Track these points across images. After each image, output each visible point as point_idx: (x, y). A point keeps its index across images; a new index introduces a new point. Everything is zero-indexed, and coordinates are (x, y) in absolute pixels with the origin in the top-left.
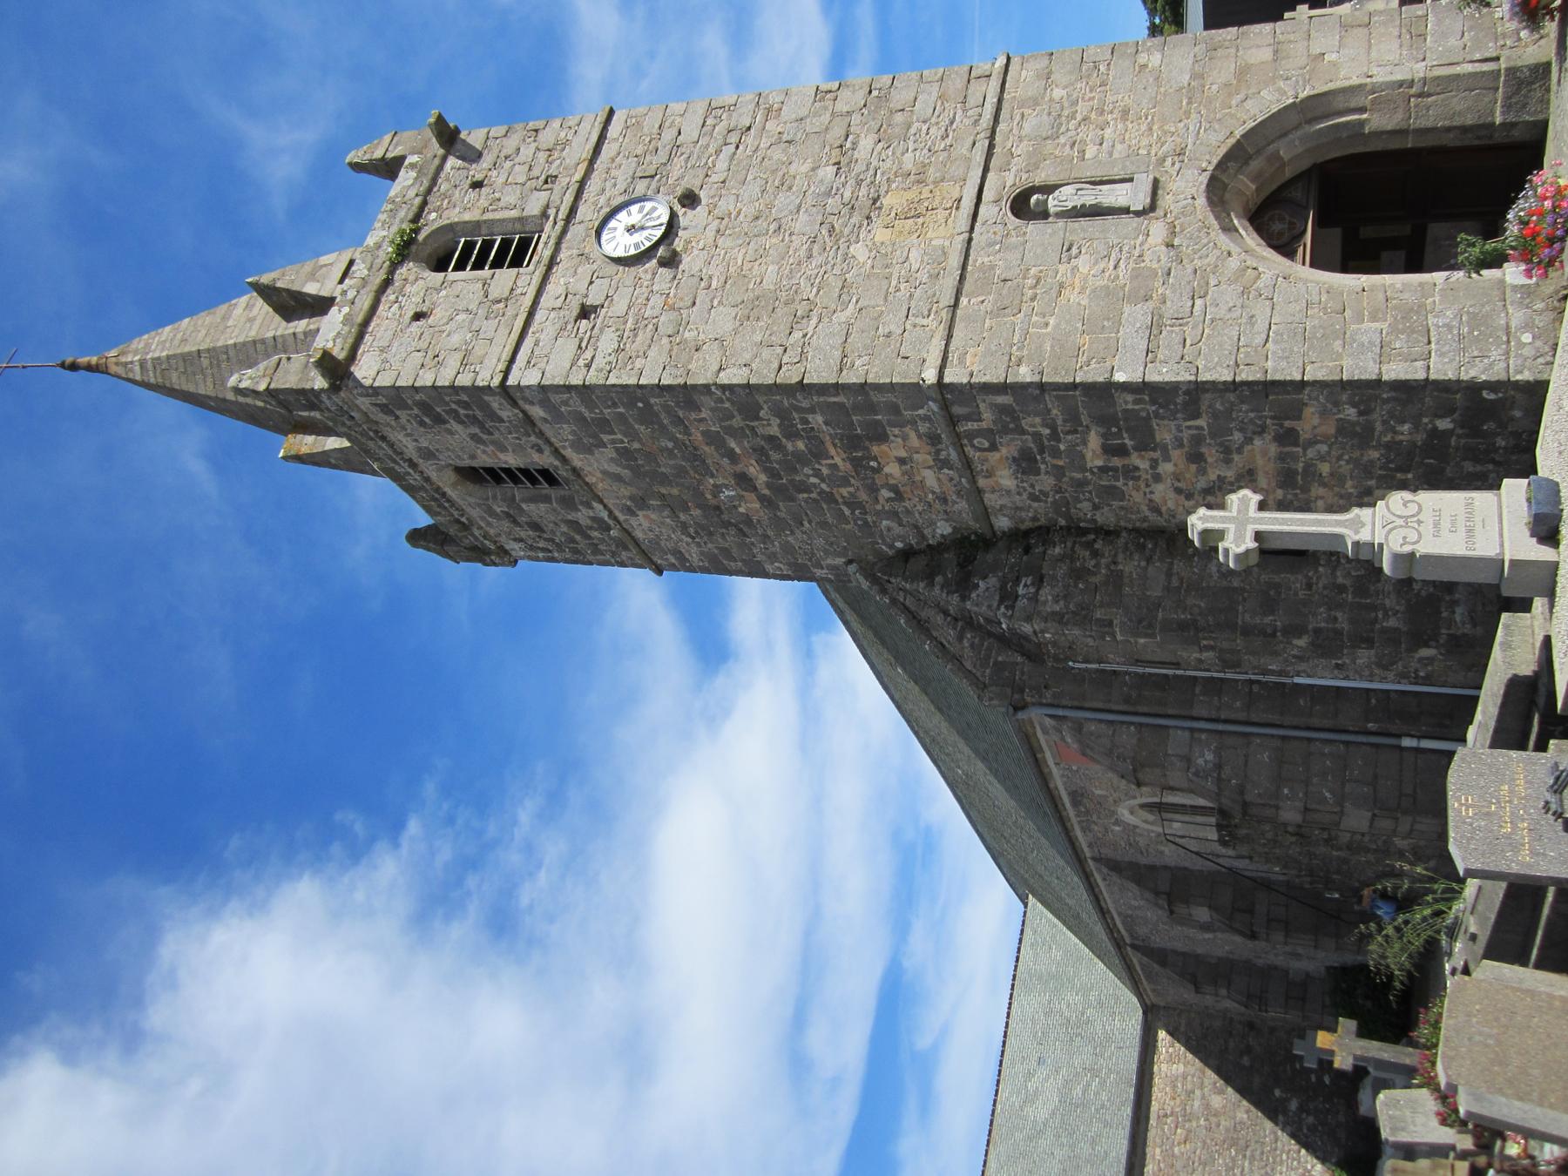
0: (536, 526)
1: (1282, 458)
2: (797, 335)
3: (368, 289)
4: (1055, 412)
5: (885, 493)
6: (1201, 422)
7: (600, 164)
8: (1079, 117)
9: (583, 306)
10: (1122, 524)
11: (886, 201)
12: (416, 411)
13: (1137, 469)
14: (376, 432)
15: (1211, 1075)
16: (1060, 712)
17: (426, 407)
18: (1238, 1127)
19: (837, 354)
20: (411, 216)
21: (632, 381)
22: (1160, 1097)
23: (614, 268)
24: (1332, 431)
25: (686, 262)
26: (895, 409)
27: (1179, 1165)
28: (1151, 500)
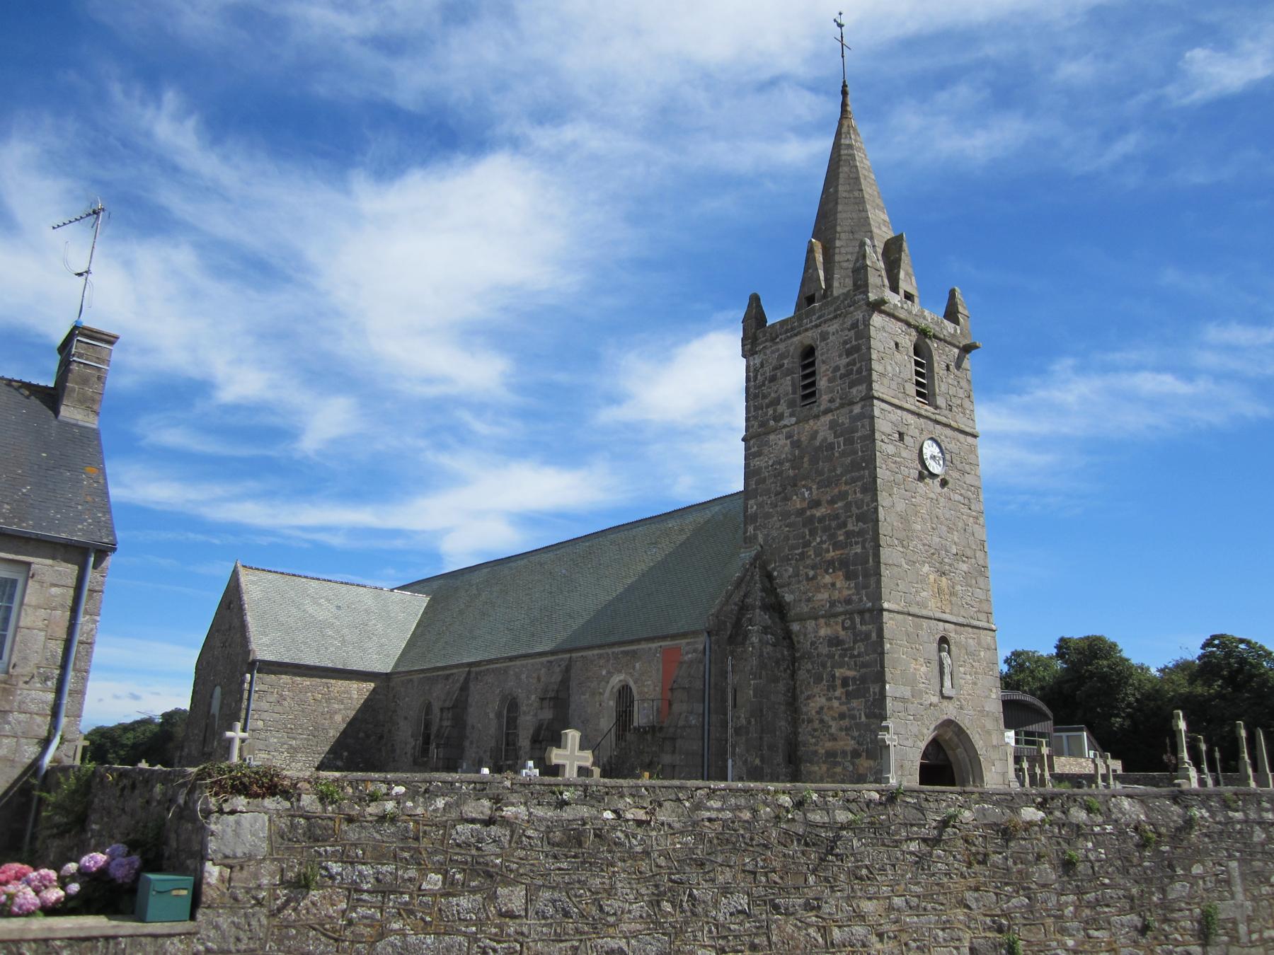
0: (773, 379)
1: (844, 753)
2: (896, 542)
3: (908, 316)
4: (868, 658)
5: (811, 573)
6: (863, 718)
7: (956, 433)
8: (974, 664)
9: (903, 434)
10: (798, 682)
11: (944, 579)
12: (854, 343)
13: (835, 691)
14: (840, 315)
15: (352, 714)
16: (707, 653)
17: (857, 349)
18: (325, 731)
19: (891, 562)
20: (936, 333)
21: (878, 464)
22: (339, 685)
23: (918, 447)
24: (860, 772)
25: (921, 484)
26: (866, 587)
27: (301, 696)
28: (815, 696)
